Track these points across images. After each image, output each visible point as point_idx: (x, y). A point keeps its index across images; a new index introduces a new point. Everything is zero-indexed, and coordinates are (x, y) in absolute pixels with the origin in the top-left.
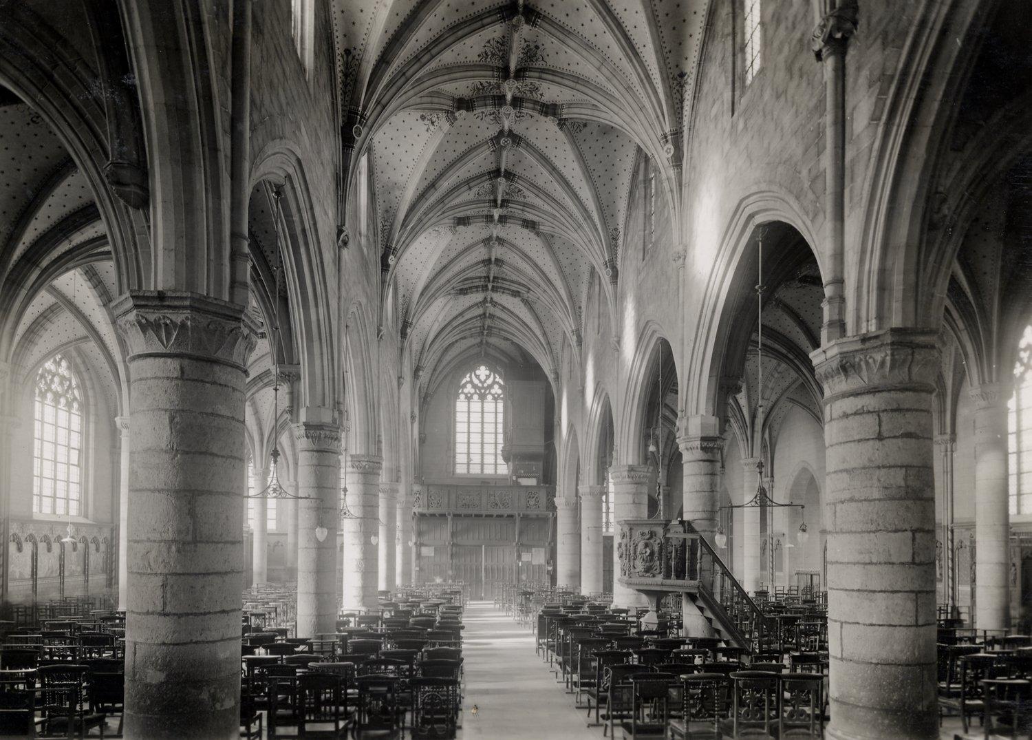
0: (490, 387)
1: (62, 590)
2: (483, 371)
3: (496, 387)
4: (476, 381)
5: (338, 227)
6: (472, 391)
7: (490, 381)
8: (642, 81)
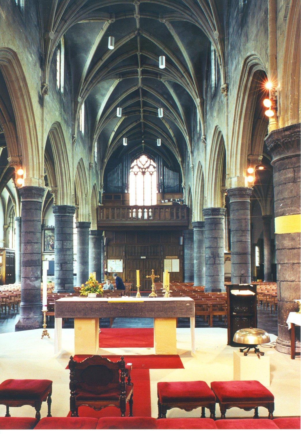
0: (148, 168)
1: (278, 249)
2: (143, 159)
3: (151, 167)
4: (140, 165)
5: (42, 84)
6: (138, 170)
7: (147, 165)
8: (226, 246)
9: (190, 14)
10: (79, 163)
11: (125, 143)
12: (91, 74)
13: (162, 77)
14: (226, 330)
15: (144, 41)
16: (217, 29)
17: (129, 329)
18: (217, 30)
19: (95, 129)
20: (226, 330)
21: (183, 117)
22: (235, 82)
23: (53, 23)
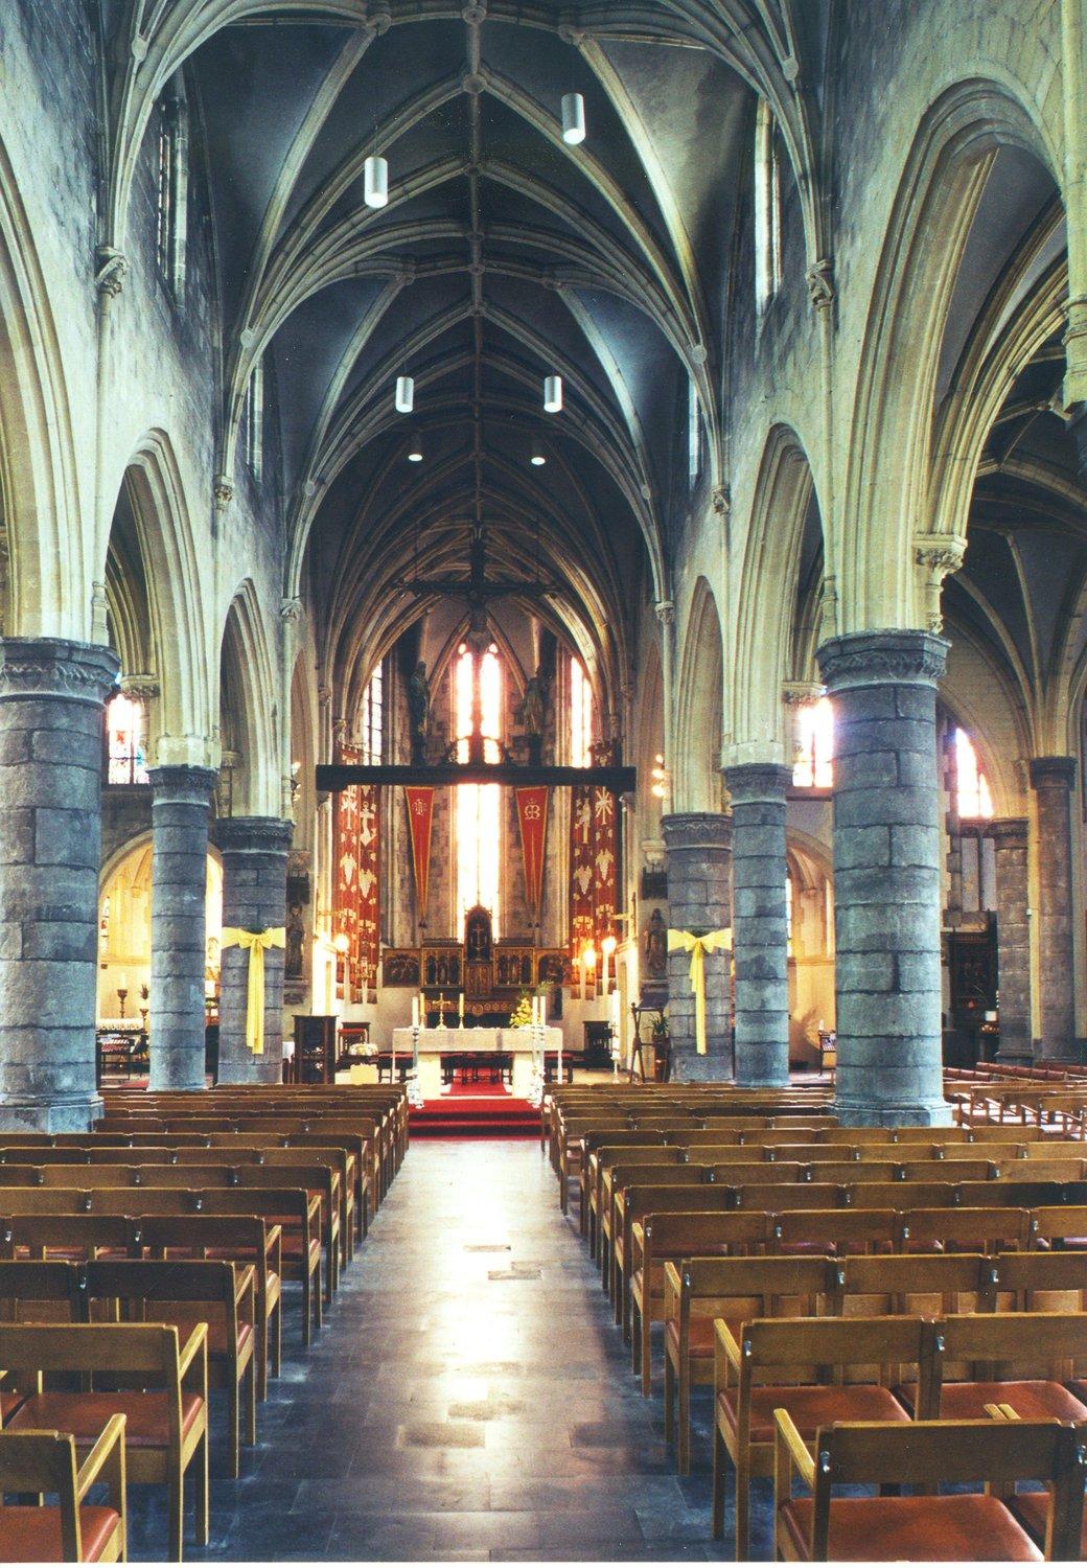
9: (668, 21)
10: (239, 598)
11: (405, 401)
12: (440, 1110)
13: (557, 273)
14: (110, 782)
15: (489, 328)
16: (792, 50)
17: (553, 562)
18: (792, 54)
19: (259, 265)
20: (110, 782)
21: (643, 456)
22: (736, 590)
23: (252, 307)
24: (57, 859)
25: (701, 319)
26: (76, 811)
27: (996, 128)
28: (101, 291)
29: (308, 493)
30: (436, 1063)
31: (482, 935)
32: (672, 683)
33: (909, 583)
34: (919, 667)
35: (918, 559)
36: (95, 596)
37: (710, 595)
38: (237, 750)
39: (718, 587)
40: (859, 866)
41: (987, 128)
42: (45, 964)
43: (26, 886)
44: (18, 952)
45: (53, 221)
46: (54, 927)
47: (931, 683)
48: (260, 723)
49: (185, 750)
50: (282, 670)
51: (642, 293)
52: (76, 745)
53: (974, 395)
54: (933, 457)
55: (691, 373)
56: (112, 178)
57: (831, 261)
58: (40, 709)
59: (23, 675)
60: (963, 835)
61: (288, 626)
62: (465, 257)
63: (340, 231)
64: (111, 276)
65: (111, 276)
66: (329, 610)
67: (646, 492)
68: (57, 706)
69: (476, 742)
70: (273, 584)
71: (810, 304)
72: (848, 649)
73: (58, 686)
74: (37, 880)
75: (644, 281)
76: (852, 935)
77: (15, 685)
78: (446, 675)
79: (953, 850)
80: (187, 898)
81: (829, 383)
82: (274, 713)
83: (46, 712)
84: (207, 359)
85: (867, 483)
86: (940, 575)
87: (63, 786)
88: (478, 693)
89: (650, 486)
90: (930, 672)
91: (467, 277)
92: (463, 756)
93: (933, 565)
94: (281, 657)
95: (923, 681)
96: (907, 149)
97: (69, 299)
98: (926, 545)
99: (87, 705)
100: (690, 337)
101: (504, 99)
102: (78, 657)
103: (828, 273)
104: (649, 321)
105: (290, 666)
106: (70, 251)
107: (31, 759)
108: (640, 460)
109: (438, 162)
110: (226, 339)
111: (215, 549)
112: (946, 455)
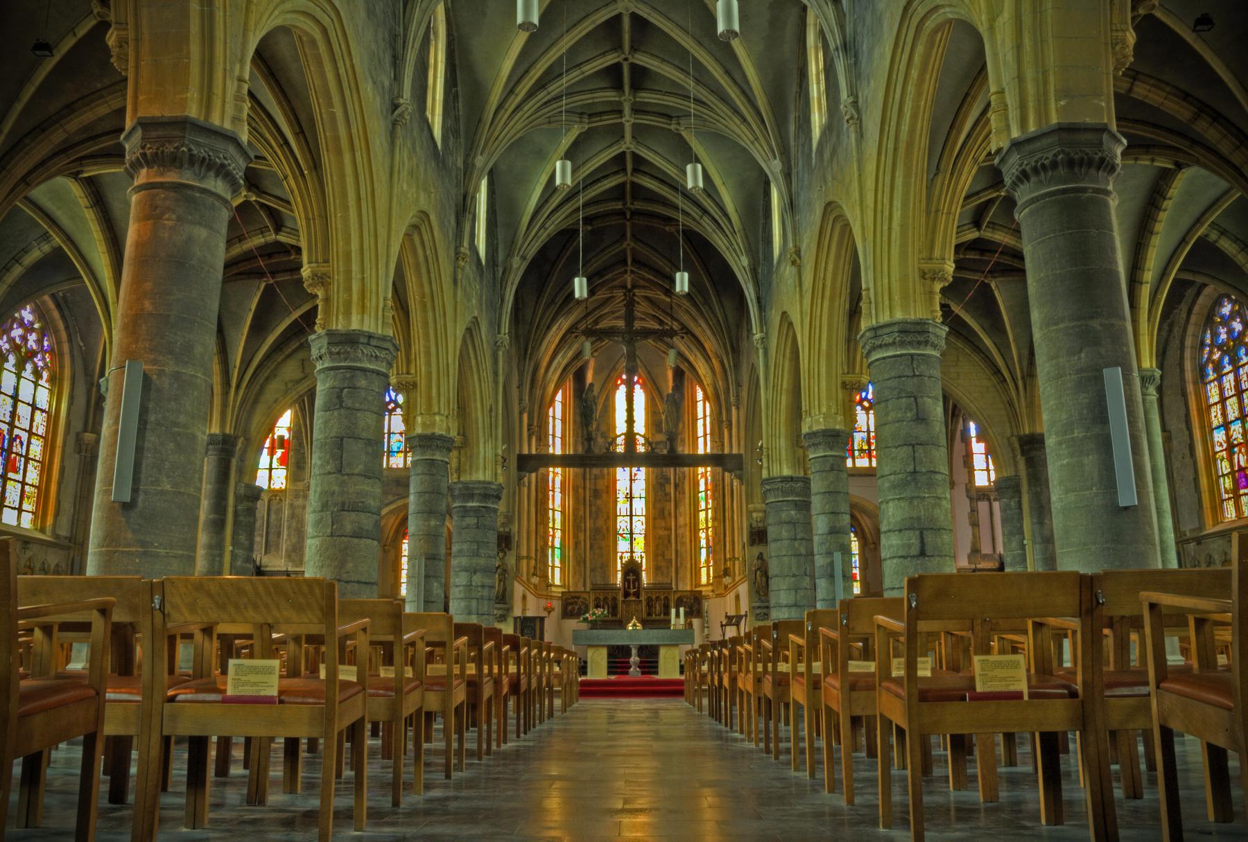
15: (637, 159)
24: (356, 471)
25: (777, 145)
26: (369, 440)
27: (947, 9)
28: (395, 123)
29: (515, 266)
30: (604, 652)
31: (634, 581)
32: (767, 388)
33: (918, 291)
34: (927, 342)
35: (923, 275)
36: (385, 306)
37: (791, 324)
38: (464, 435)
39: (795, 317)
40: (894, 473)
41: (942, 11)
42: (346, 539)
43: (336, 488)
44: (329, 531)
45: (370, 81)
46: (353, 516)
47: (936, 353)
48: (478, 413)
49: (433, 424)
50: (496, 382)
51: (738, 131)
52: (370, 398)
53: (952, 174)
54: (928, 213)
55: (771, 178)
56: (403, 59)
57: (857, 97)
58: (348, 375)
59: (338, 353)
60: (979, 499)
61: (500, 353)
62: (620, 112)
63: (540, 97)
64: (401, 115)
65: (401, 115)
66: (526, 351)
67: (745, 261)
68: (358, 373)
69: (630, 436)
70: (491, 324)
71: (846, 125)
72: (879, 332)
73: (360, 360)
74: (342, 484)
75: (738, 122)
76: (891, 520)
77: (333, 360)
78: (607, 399)
79: (972, 511)
80: (433, 523)
81: (859, 169)
82: (491, 410)
83: (352, 377)
84: (454, 174)
85: (886, 227)
86: (938, 286)
87: (362, 424)
88: (630, 411)
89: (748, 256)
90: (934, 346)
91: (622, 125)
92: (620, 449)
93: (933, 279)
94: (496, 374)
95: (929, 351)
96: (897, 25)
97: (377, 128)
98: (926, 267)
99: (378, 373)
100: (770, 155)
101: (645, 16)
102: (374, 342)
103: (855, 104)
104: (744, 150)
105: (501, 379)
106: (378, 99)
107: (341, 406)
108: (739, 240)
109: (604, 54)
110: (465, 163)
111: (455, 294)
112: (937, 211)
